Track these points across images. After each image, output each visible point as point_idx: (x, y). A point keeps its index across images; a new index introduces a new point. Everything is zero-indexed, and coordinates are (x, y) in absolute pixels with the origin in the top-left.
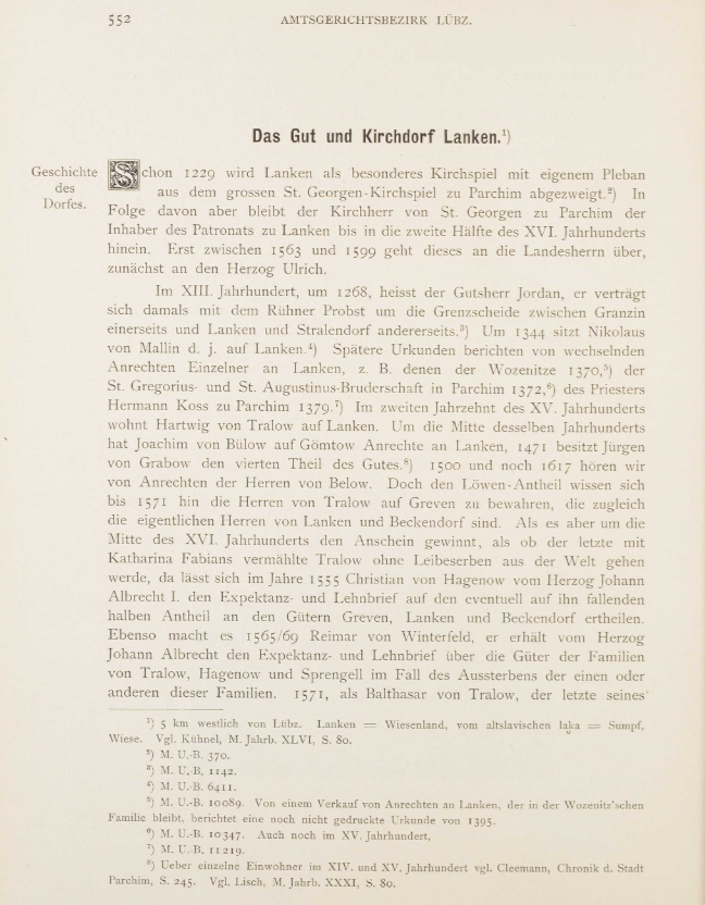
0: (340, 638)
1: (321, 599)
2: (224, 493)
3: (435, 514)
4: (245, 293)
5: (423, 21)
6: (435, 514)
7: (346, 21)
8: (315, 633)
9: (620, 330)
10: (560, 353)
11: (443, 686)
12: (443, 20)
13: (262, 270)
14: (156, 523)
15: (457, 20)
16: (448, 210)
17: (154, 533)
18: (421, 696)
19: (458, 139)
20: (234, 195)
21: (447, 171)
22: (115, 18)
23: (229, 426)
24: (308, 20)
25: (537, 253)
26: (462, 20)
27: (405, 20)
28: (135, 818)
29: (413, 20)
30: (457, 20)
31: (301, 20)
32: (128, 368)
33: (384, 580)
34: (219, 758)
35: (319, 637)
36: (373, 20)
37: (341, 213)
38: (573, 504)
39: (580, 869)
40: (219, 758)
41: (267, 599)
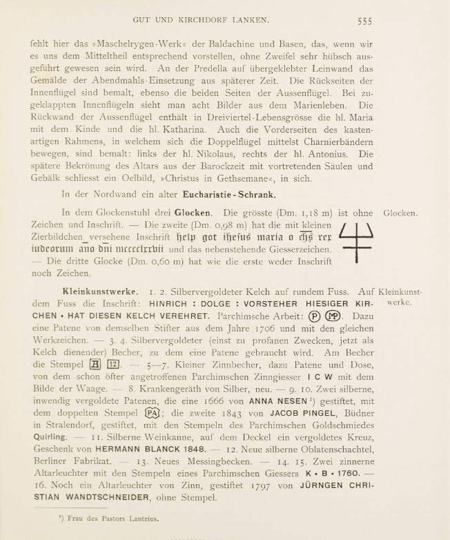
0: (173, 106)
3: (69, 334)
6: (69, 334)
9: (217, 153)
11: (290, 220)
14: (253, 144)
19: (136, 520)
20: (248, 215)
22: (362, 20)
23: (236, 402)
34: (260, 488)
40: (260, 488)
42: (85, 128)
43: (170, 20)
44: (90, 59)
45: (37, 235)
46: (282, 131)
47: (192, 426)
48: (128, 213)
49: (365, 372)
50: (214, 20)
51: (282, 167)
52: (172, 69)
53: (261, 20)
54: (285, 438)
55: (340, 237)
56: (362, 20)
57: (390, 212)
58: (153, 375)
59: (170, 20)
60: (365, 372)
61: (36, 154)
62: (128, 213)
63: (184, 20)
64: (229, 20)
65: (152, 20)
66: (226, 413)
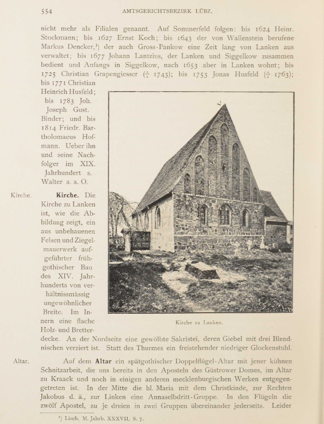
0: (73, 295)
1: (51, 155)
5: (189, 11)
7: (153, 11)
8: (269, 386)
12: (198, 11)
15: (205, 11)
17: (133, 385)
18: (231, 362)
22: (44, 11)
24: (135, 11)
26: (207, 11)
27: (181, 11)
29: (185, 11)
30: (205, 11)
31: (132, 11)
32: (72, 38)
33: (79, 74)
35: (271, 388)
36: (166, 11)
41: (113, 348)
42: (63, 194)
44: (45, 49)
45: (79, 239)
47: (47, 38)
51: (61, 286)
52: (78, 339)
54: (64, 321)
55: (294, 92)
56: (44, 11)
57: (256, 347)
66: (44, 128)
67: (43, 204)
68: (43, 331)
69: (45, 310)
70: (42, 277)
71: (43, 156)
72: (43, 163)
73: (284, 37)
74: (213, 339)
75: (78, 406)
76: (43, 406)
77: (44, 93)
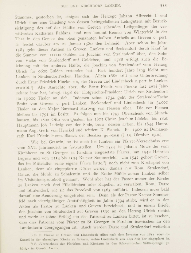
2: (84, 84)
4: (46, 148)
10: (28, 222)
13: (138, 211)
16: (49, 152)
21: (22, 152)
22: (162, 5)
25: (23, 228)
28: (28, 240)
37: (93, 244)
38: (83, 87)
39: (25, 240)
43: (77, 6)
46: (101, 169)
48: (90, 235)
49: (167, 219)
50: (96, 6)
53: (117, 5)
58: (151, 167)
59: (77, 6)
60: (167, 219)
61: (98, 125)
62: (90, 235)
63: (83, 6)
64: (103, 6)
65: (69, 6)
66: (161, 118)
67: (18, 153)
68: (84, 93)
69: (159, 204)
70: (154, 147)
71: (20, 218)
72: (82, 113)
73: (88, 168)
74: (61, 66)
75: (83, 147)
76: (151, 87)
77: (103, 17)
